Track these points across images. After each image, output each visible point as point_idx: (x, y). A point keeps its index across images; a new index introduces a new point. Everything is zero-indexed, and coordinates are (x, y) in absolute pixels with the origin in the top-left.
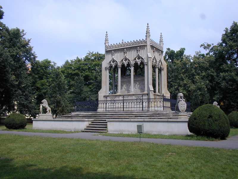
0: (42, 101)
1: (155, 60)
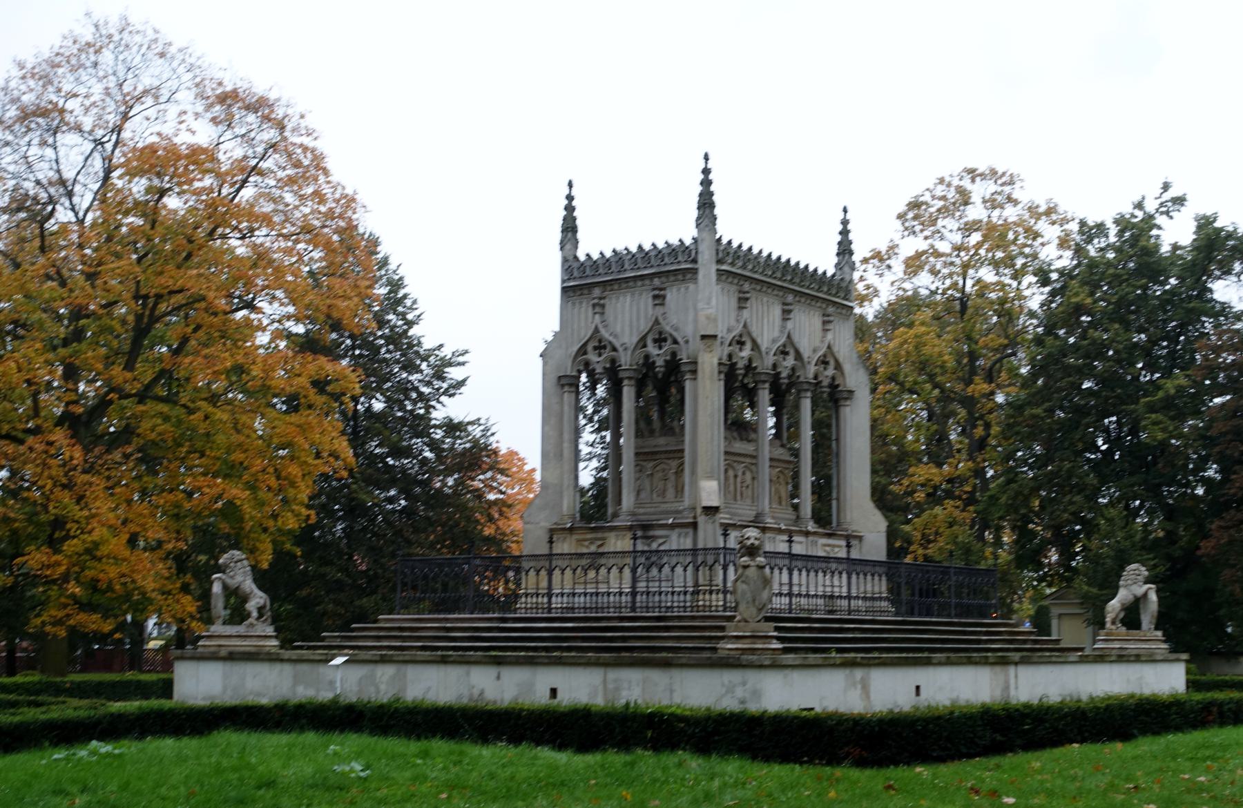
0: (221, 561)
1: (792, 352)
